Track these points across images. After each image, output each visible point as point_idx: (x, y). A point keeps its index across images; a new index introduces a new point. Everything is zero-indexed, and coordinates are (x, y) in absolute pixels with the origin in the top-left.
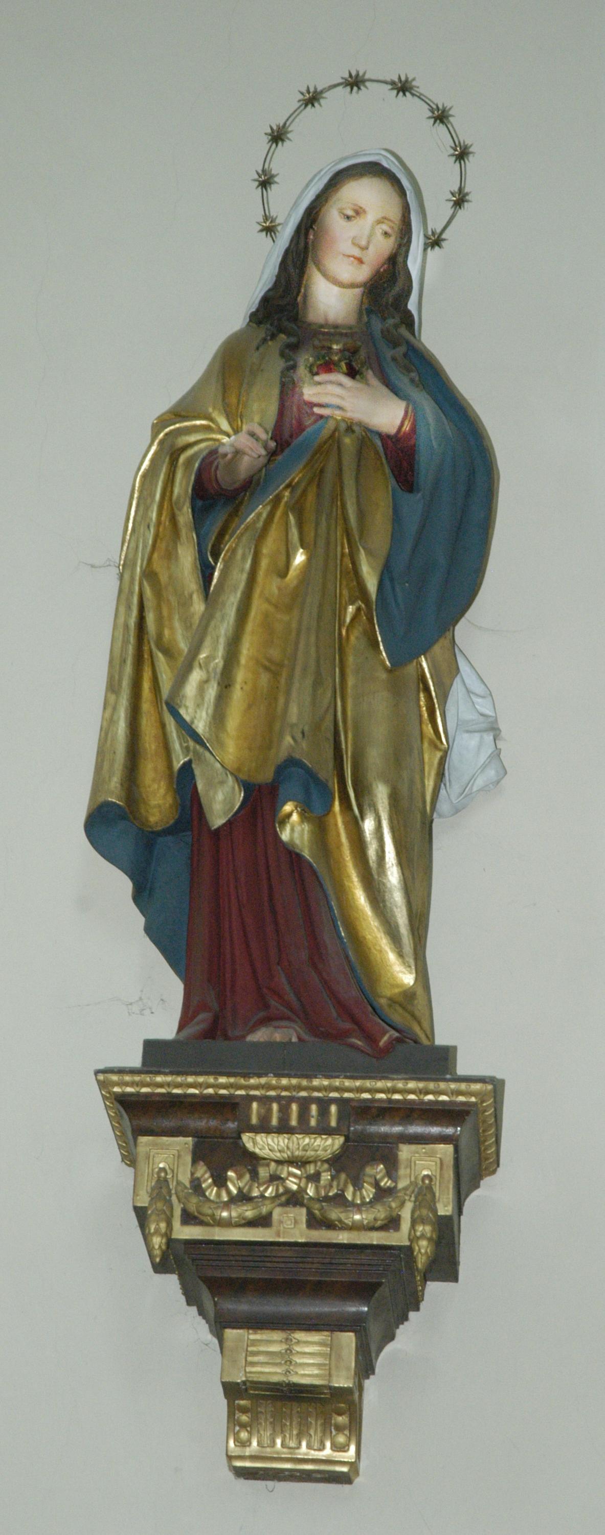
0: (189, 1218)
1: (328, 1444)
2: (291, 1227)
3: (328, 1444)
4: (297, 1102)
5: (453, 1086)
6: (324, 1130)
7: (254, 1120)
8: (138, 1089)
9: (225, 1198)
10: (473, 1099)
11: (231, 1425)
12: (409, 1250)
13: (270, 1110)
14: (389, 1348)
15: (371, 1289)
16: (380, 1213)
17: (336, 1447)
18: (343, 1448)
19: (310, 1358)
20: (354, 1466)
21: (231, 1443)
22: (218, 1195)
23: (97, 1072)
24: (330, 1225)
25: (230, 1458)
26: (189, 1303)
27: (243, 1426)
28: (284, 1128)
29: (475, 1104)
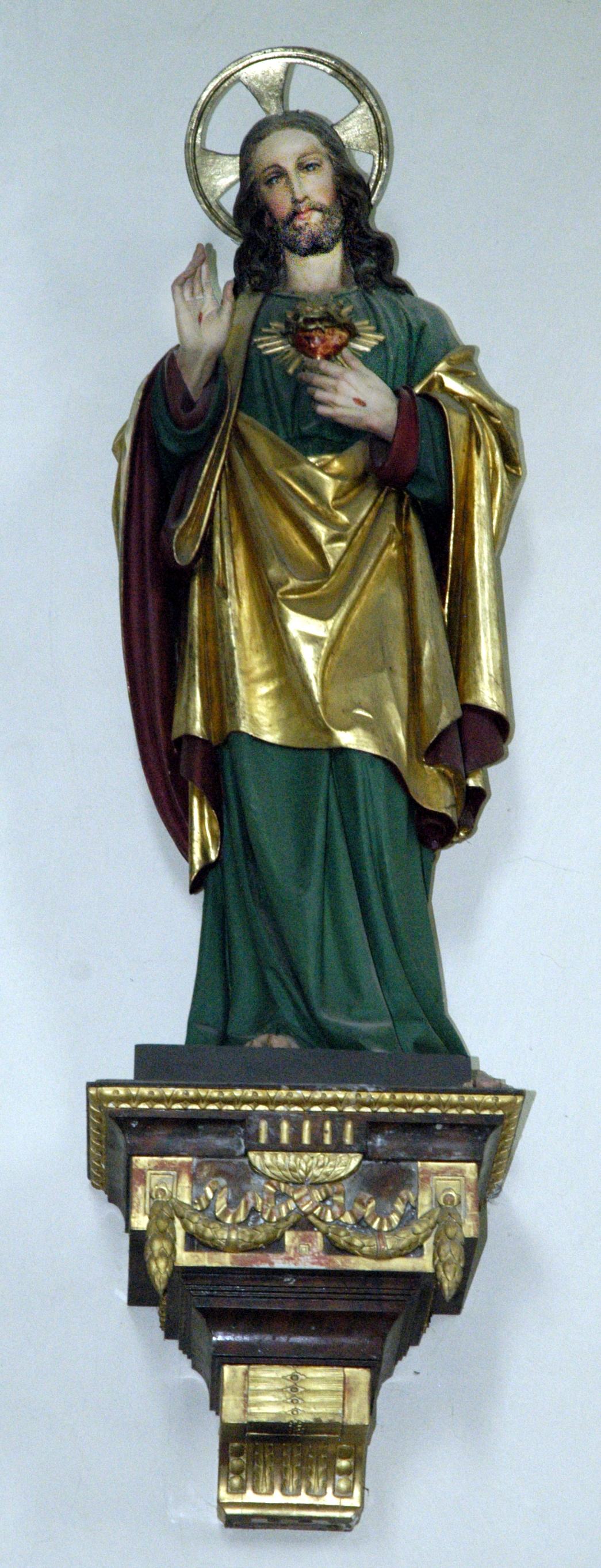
0: (194, 1242)
1: (330, 1490)
2: (302, 1254)
3: (330, 1490)
4: (352, 1119)
5: (477, 1098)
6: (338, 1147)
7: (263, 1139)
8: (272, 1108)
9: (229, 1220)
10: (500, 1113)
11: (224, 1472)
12: (434, 1277)
13: (322, 1130)
14: (389, 1381)
15: (374, 1317)
16: (405, 1238)
17: (338, 1493)
18: (349, 1493)
19: (321, 1393)
20: (358, 1511)
21: (223, 1488)
22: (381, 1224)
23: (90, 1085)
24: (346, 1251)
25: (221, 1505)
26: (168, 1336)
27: (238, 1473)
28: (296, 1147)
29: (502, 1117)
